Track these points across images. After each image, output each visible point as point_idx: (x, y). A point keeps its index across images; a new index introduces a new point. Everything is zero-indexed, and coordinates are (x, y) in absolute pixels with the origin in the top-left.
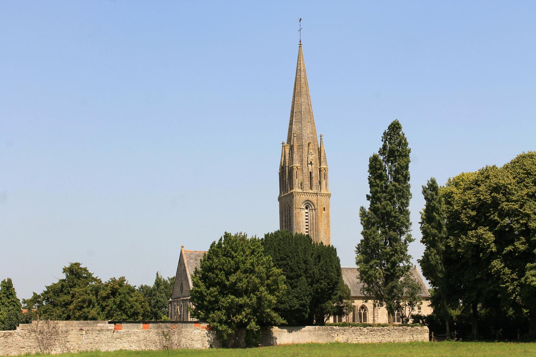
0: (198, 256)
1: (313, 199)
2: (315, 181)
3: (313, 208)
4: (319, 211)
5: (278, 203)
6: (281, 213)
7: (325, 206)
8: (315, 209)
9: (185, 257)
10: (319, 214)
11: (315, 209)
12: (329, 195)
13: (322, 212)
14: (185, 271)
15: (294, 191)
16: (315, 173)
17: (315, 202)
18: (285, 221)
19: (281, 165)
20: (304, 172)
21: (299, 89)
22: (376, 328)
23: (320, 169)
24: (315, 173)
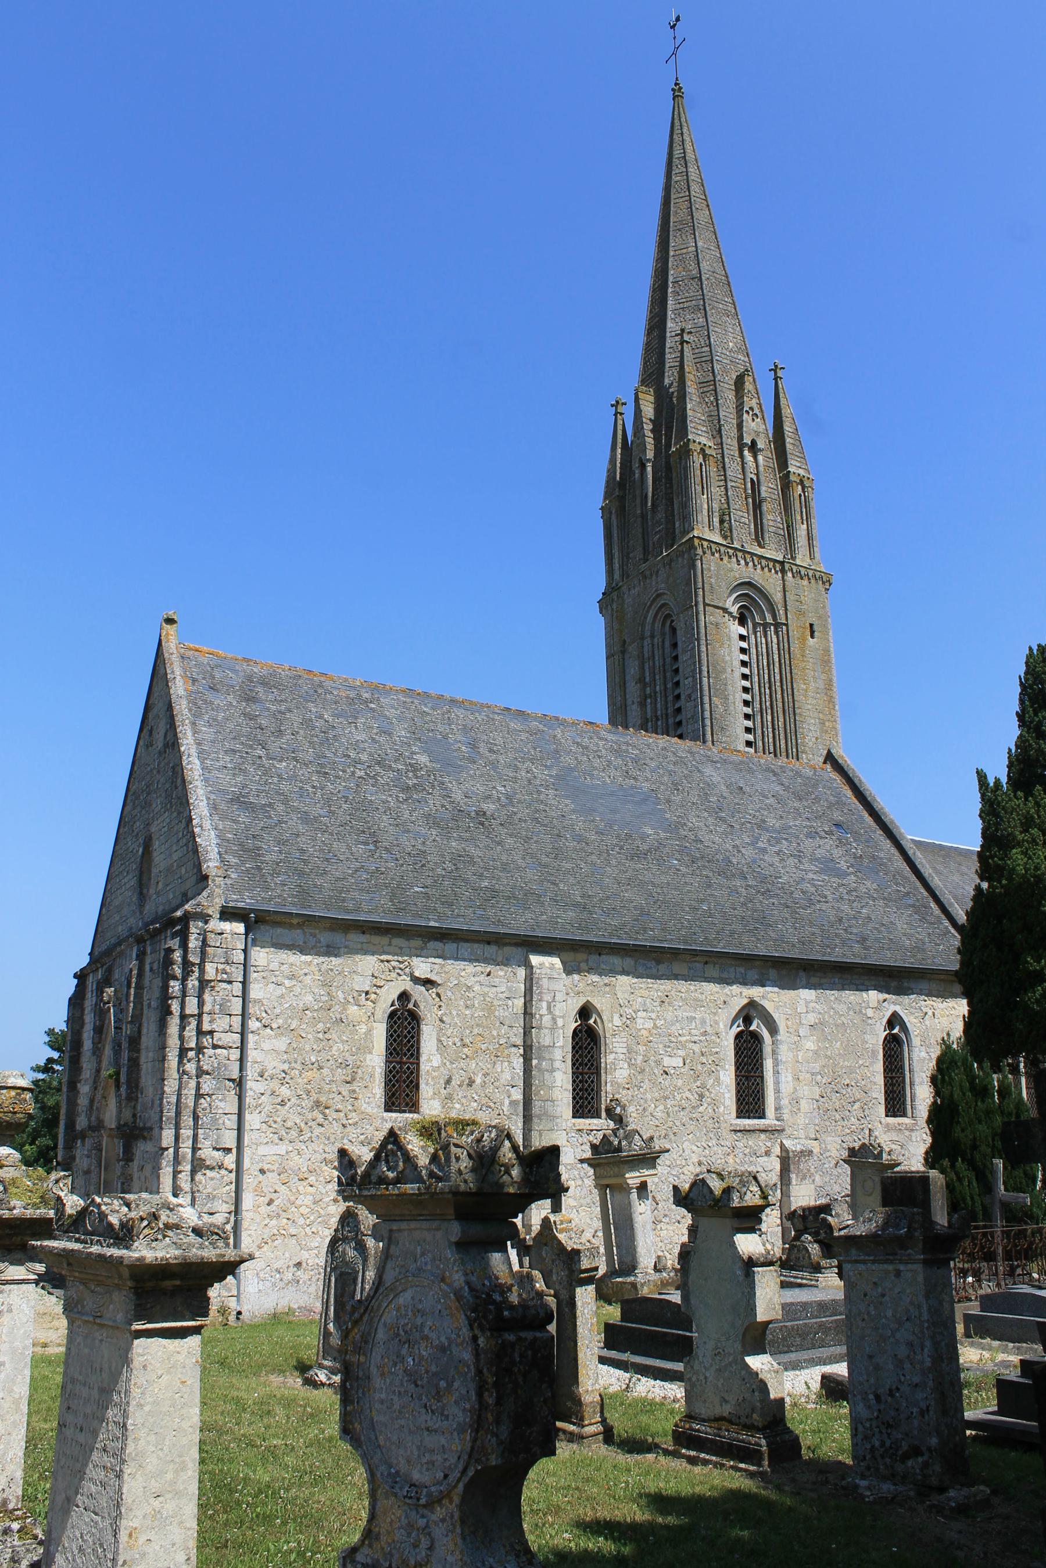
0: (264, 683)
1: (770, 582)
2: (772, 518)
3: (769, 619)
4: (794, 633)
5: (601, 621)
6: (618, 653)
7: (814, 621)
8: (777, 625)
9: (179, 688)
10: (795, 647)
11: (777, 625)
12: (825, 581)
13: (804, 640)
14: (172, 744)
15: (696, 533)
16: (769, 488)
17: (778, 597)
18: (641, 680)
19: (611, 472)
20: (729, 473)
21: (674, 162)
22: (125, 1055)
23: (197, 1232)
24: (769, 488)
